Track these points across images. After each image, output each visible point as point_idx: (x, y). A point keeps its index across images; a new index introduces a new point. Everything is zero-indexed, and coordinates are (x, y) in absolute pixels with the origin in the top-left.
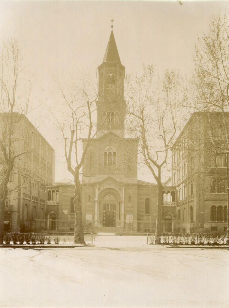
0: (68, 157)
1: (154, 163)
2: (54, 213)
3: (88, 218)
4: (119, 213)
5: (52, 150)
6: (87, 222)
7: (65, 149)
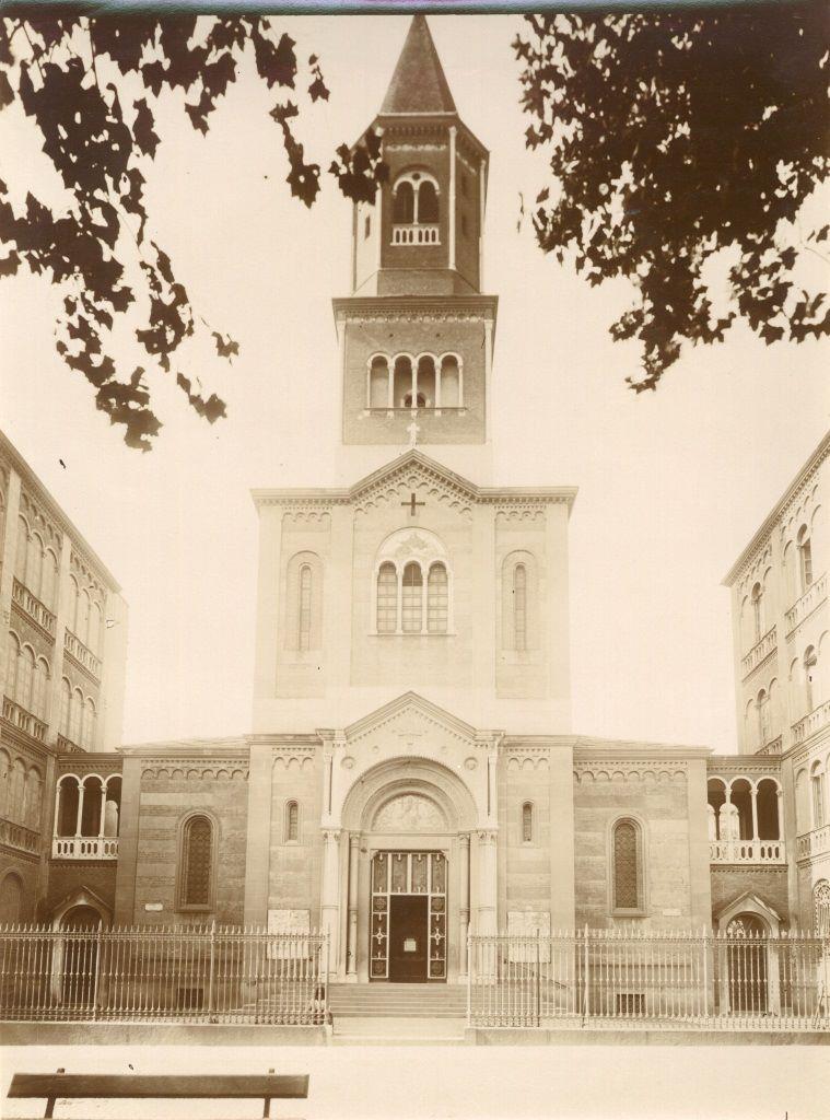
2: (95, 905)
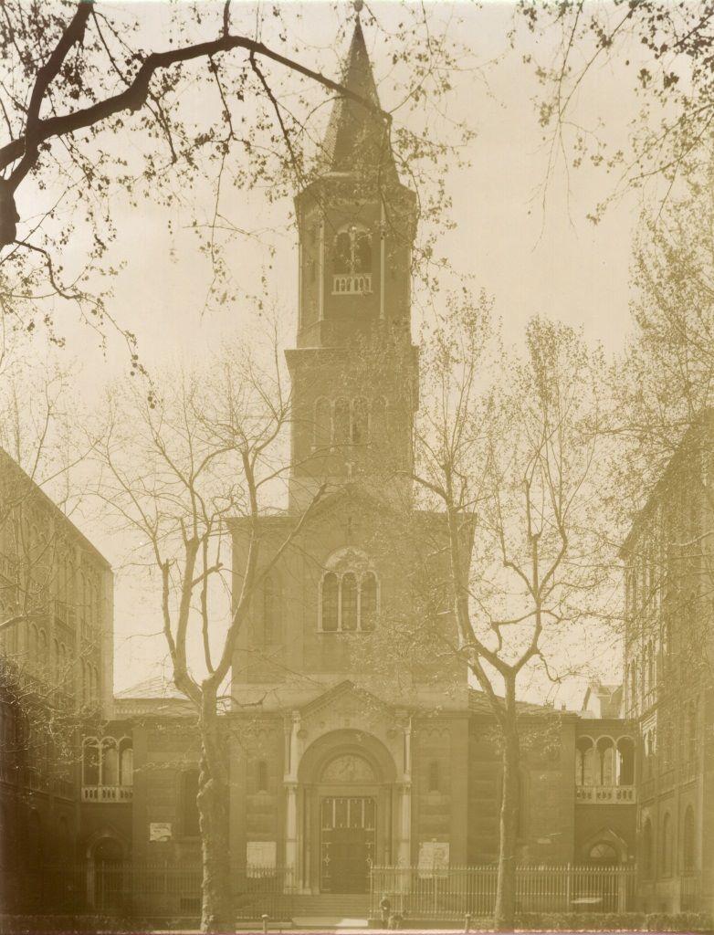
0: (174, 637)
1: (493, 658)
3: (260, 855)
4: (387, 835)
5: (95, 567)
6: (250, 875)
7: (165, 608)
